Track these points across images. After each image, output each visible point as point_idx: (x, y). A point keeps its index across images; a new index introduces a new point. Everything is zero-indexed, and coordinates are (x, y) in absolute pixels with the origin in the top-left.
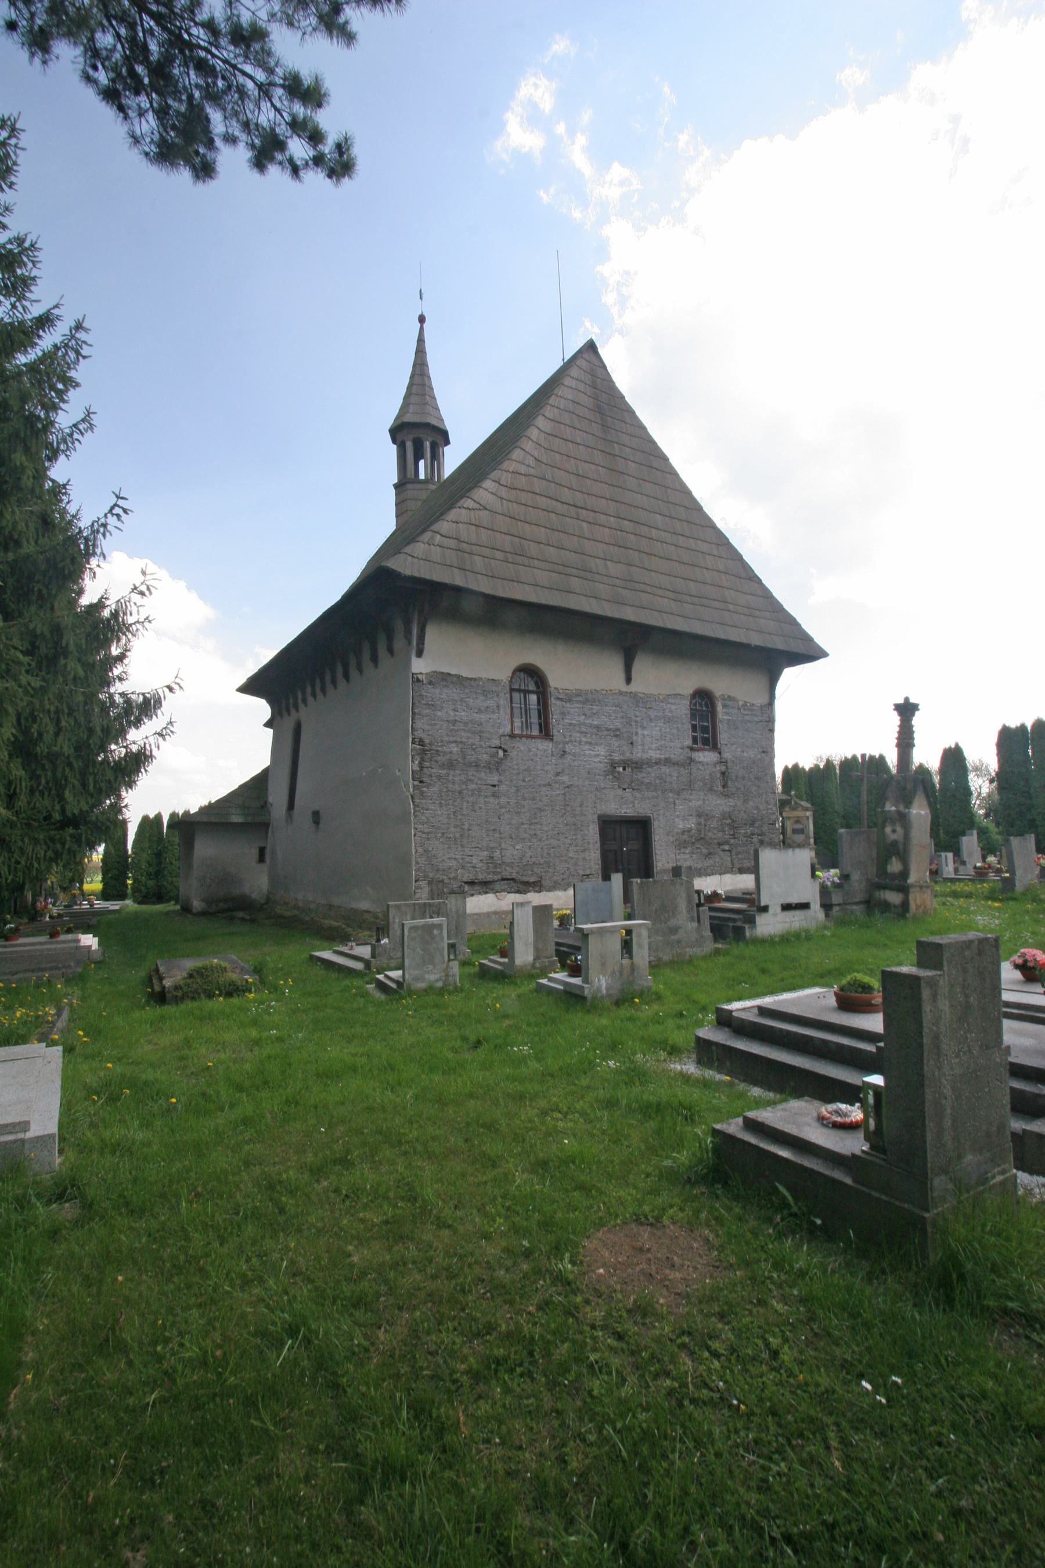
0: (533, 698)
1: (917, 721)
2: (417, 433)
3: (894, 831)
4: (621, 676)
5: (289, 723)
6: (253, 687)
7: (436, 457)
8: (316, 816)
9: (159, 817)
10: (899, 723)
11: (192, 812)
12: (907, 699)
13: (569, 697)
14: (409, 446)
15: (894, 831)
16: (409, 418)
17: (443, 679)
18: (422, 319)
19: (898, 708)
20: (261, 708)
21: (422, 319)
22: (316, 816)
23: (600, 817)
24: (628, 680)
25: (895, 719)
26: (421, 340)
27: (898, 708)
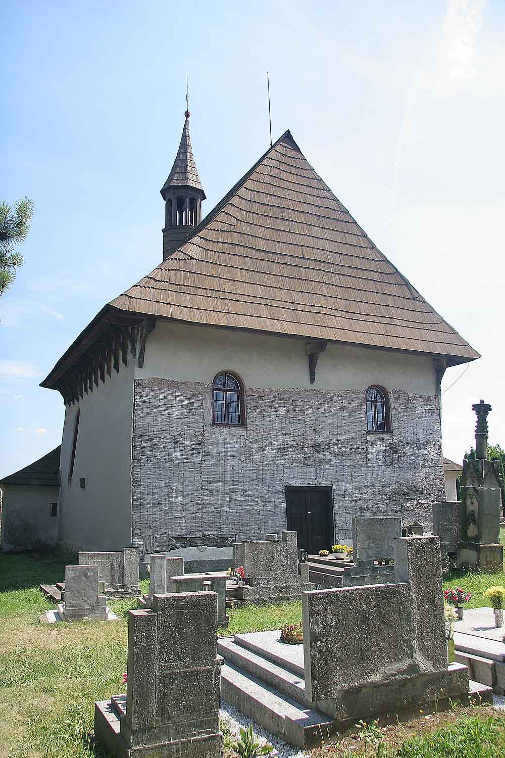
0: (233, 396)
1: (490, 418)
2: (180, 196)
3: (472, 503)
4: (307, 377)
5: (74, 408)
6: (49, 383)
7: (193, 209)
8: (83, 482)
9: (464, 460)
10: (477, 420)
11: (475, 448)
12: (482, 401)
13: (261, 395)
14: (174, 203)
15: (472, 503)
16: (174, 183)
17: (157, 383)
18: (187, 114)
19: (475, 407)
20: (55, 397)
21: (187, 114)
22: (83, 482)
23: (286, 487)
24: (312, 379)
25: (474, 417)
26: (185, 129)
27: (475, 407)
